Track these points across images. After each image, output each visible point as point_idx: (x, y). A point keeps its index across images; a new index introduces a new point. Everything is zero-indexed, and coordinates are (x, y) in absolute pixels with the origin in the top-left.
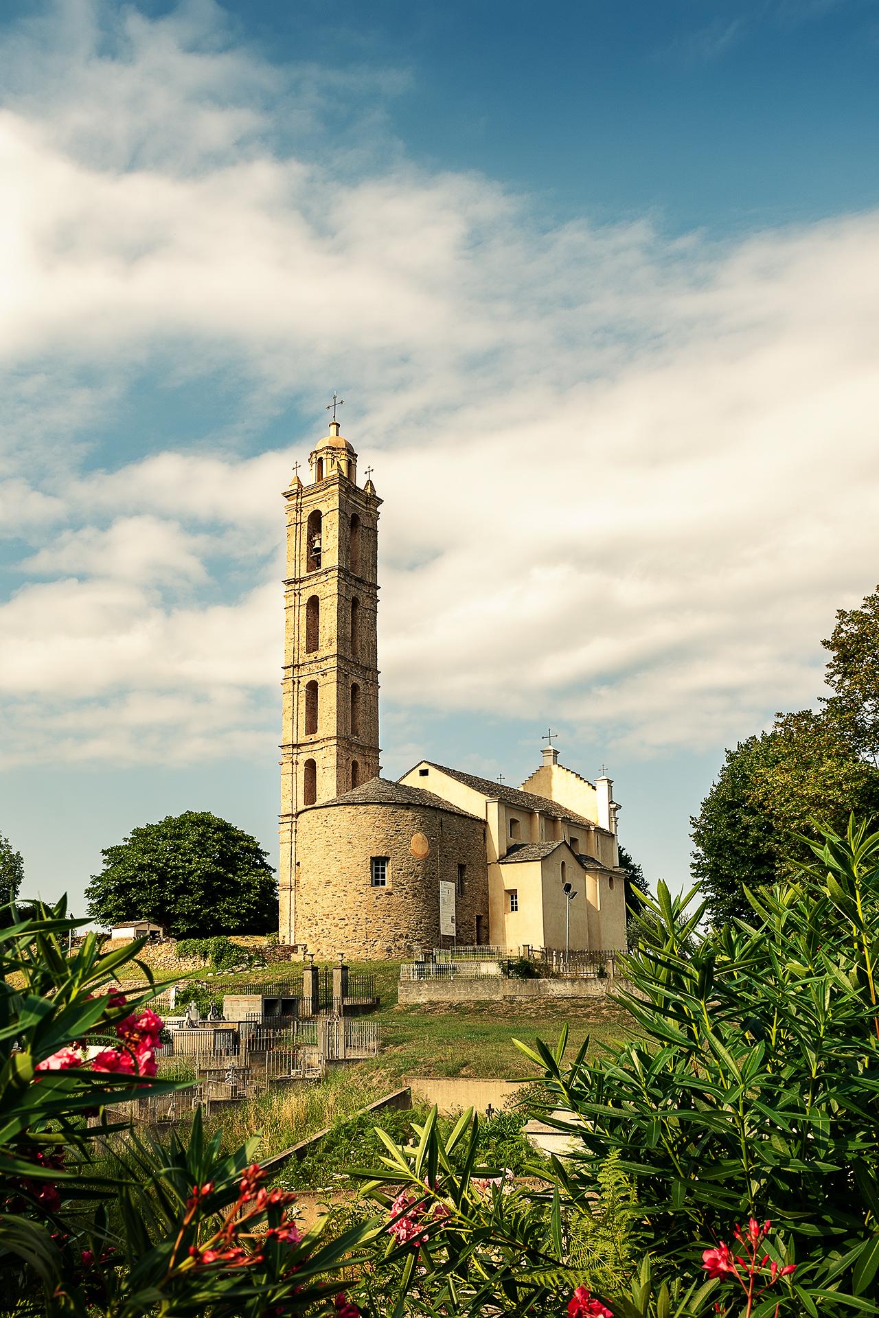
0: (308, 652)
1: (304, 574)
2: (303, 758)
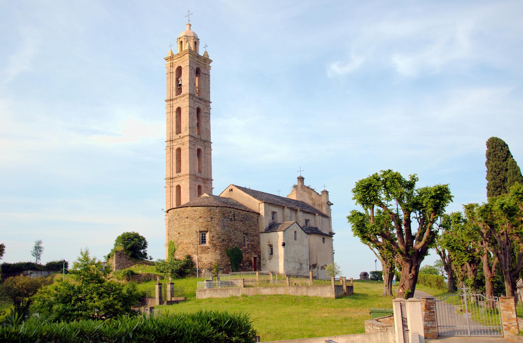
0: (177, 133)
1: (175, 97)
2: (175, 184)
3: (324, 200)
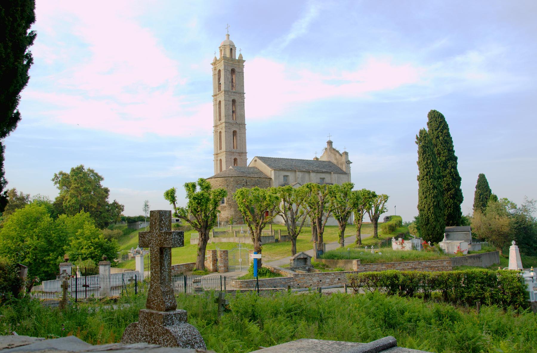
2: (219, 158)
3: (344, 159)
